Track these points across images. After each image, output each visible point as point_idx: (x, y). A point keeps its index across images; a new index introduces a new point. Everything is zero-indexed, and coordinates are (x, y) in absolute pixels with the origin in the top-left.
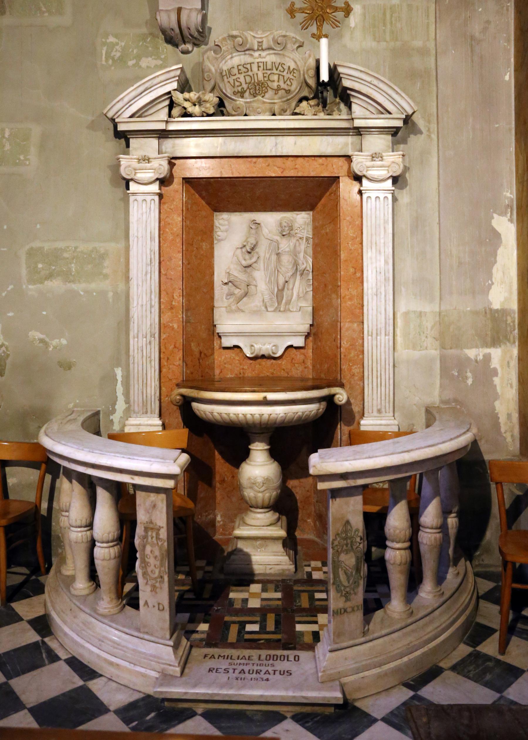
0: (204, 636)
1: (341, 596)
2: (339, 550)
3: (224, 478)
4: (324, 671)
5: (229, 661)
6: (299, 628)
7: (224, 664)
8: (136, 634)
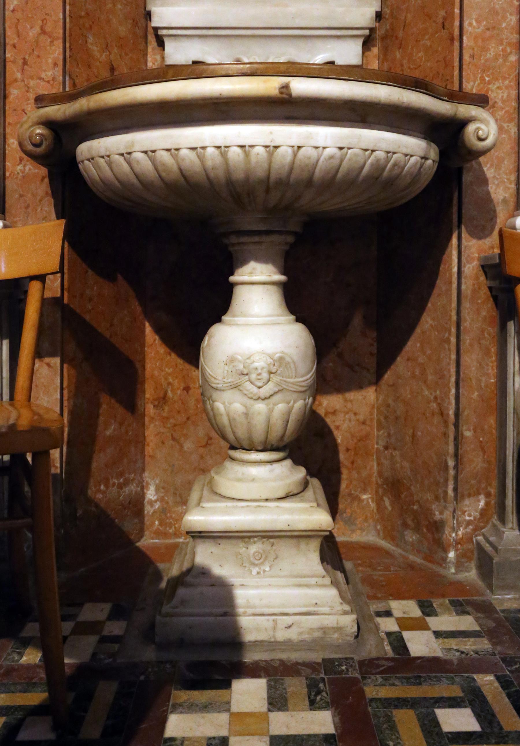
3: (166, 393)
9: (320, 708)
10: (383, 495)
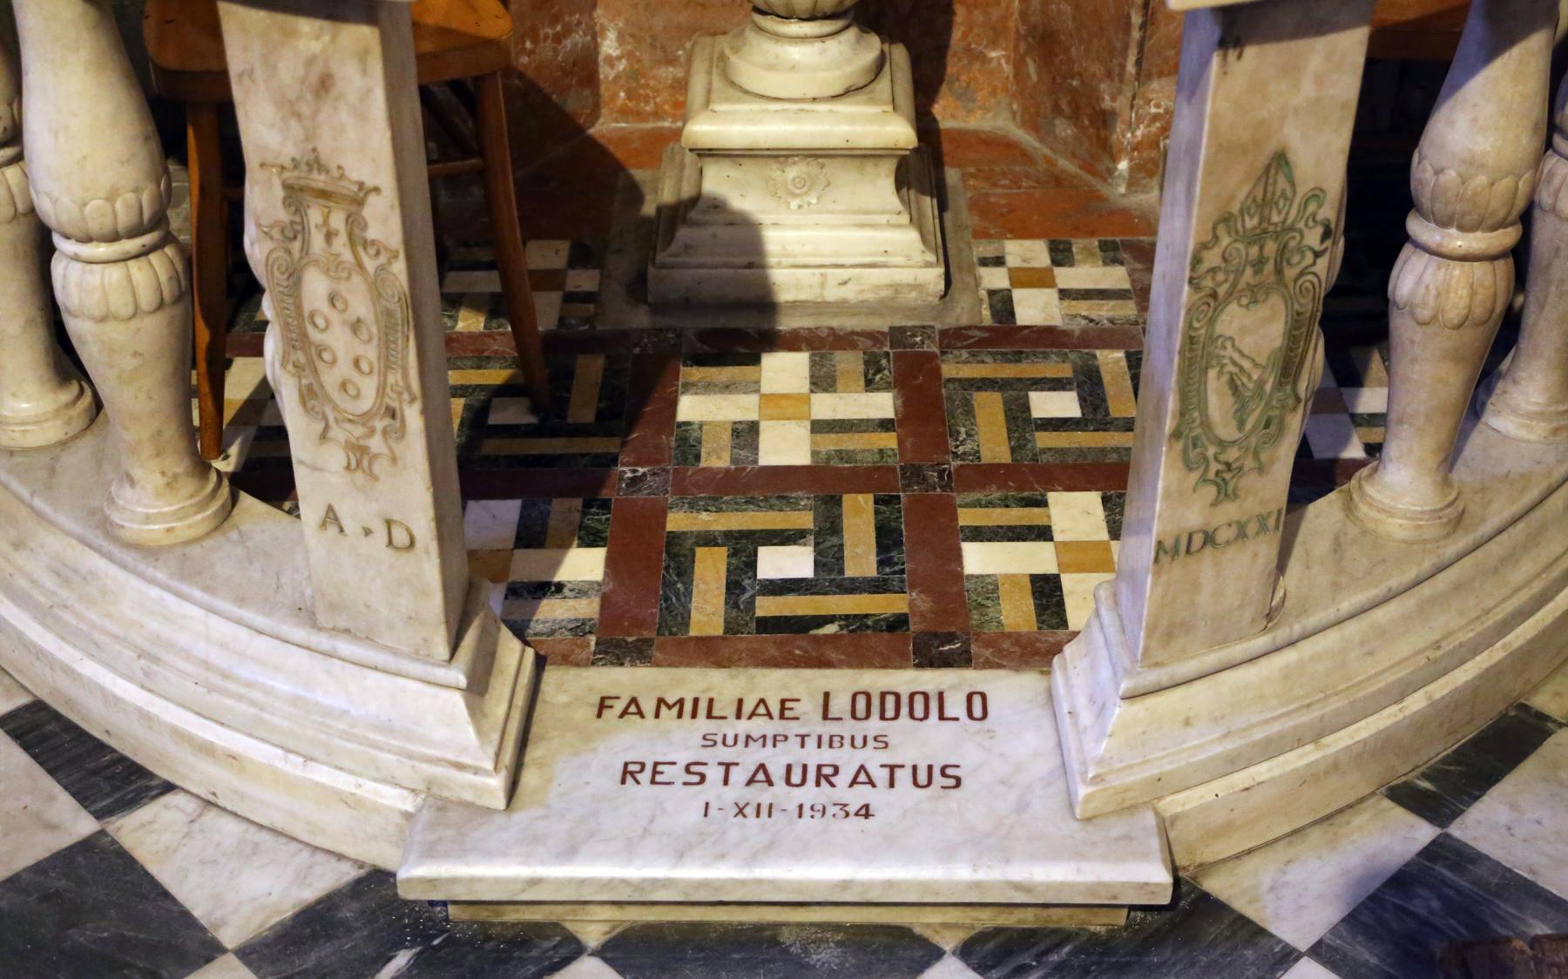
0: (588, 608)
1: (1204, 480)
2: (1221, 291)
4: (1098, 779)
5: (703, 724)
6: (978, 559)
7: (679, 741)
8: (301, 634)
9: (878, 390)
10: (1025, 54)
